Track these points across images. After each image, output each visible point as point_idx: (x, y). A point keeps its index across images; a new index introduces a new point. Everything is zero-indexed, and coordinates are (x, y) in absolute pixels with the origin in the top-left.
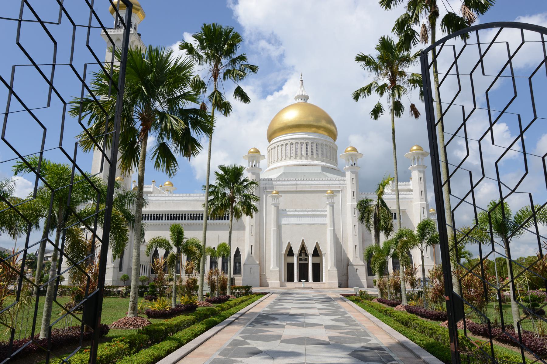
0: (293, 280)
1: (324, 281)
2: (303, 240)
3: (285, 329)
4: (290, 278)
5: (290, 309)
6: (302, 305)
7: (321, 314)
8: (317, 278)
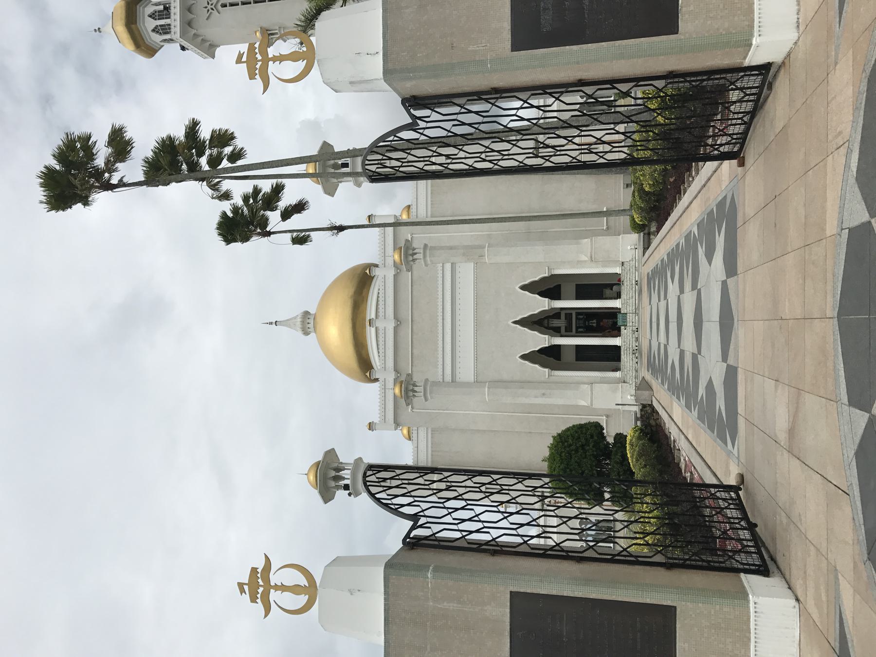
0: (617, 349)
1: (618, 270)
2: (515, 322)
3: (686, 349)
4: (610, 357)
5: (659, 344)
6: (673, 326)
7: (694, 286)
8: (603, 286)
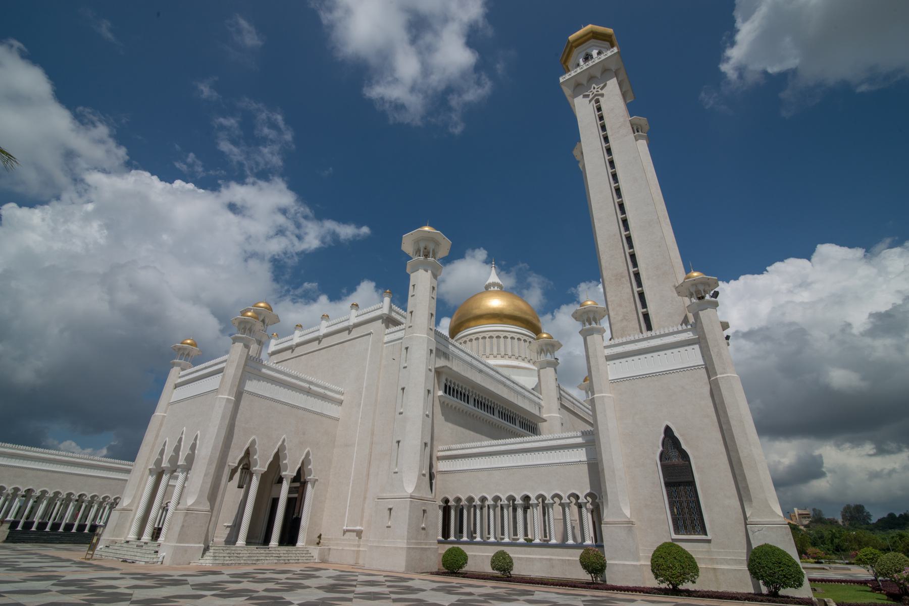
1: (300, 543)
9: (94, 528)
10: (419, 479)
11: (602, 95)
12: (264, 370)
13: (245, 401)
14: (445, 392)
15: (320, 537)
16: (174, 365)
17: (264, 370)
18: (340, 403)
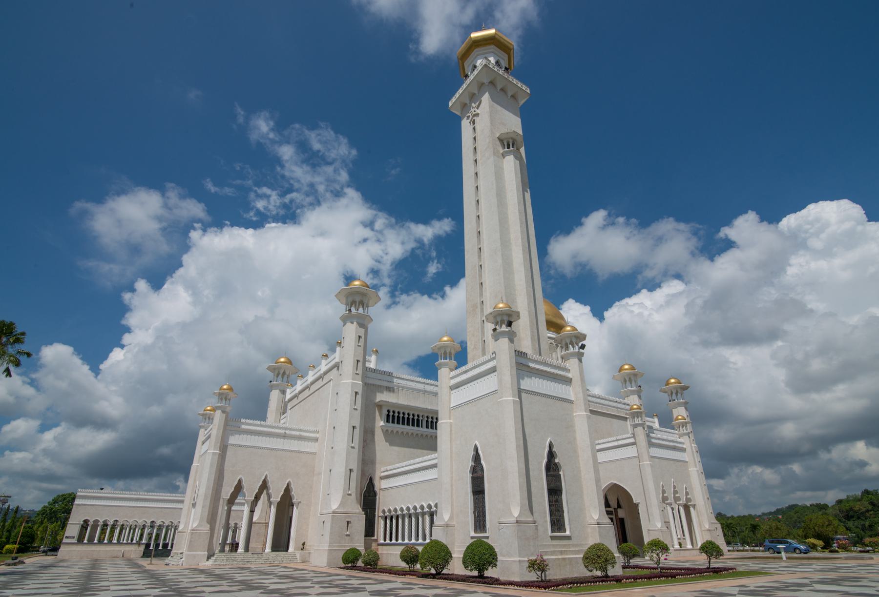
1: (291, 549)
9: (165, 546)
10: (343, 497)
11: (477, 115)
12: (243, 427)
13: (230, 453)
14: (388, 421)
15: (304, 544)
16: (441, 365)
17: (243, 427)
18: (316, 440)
